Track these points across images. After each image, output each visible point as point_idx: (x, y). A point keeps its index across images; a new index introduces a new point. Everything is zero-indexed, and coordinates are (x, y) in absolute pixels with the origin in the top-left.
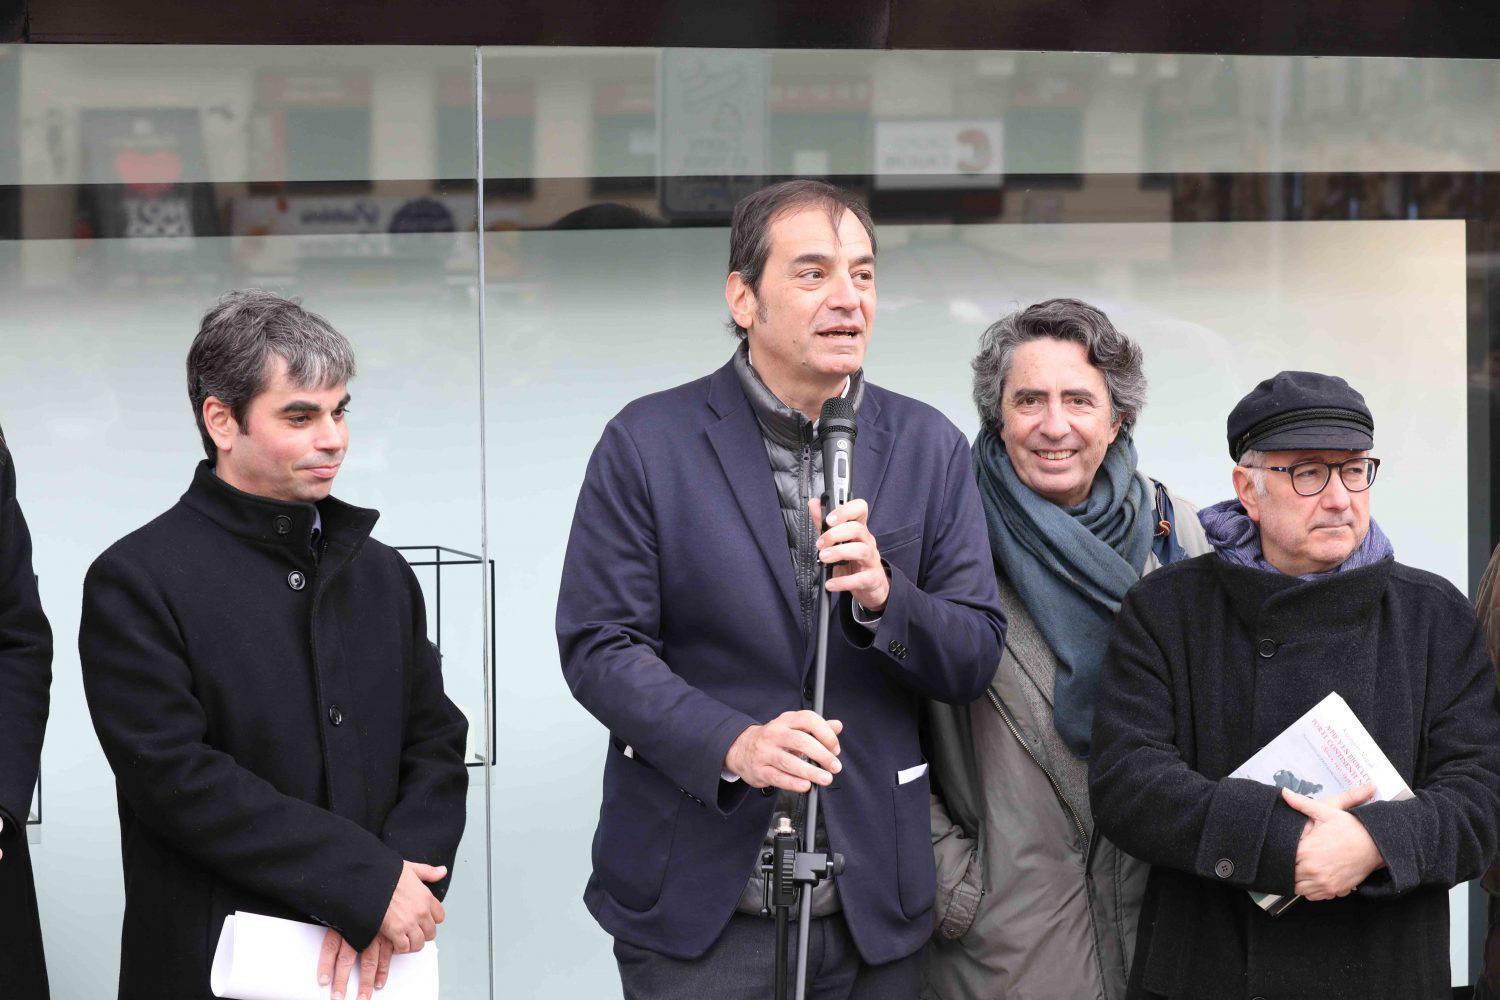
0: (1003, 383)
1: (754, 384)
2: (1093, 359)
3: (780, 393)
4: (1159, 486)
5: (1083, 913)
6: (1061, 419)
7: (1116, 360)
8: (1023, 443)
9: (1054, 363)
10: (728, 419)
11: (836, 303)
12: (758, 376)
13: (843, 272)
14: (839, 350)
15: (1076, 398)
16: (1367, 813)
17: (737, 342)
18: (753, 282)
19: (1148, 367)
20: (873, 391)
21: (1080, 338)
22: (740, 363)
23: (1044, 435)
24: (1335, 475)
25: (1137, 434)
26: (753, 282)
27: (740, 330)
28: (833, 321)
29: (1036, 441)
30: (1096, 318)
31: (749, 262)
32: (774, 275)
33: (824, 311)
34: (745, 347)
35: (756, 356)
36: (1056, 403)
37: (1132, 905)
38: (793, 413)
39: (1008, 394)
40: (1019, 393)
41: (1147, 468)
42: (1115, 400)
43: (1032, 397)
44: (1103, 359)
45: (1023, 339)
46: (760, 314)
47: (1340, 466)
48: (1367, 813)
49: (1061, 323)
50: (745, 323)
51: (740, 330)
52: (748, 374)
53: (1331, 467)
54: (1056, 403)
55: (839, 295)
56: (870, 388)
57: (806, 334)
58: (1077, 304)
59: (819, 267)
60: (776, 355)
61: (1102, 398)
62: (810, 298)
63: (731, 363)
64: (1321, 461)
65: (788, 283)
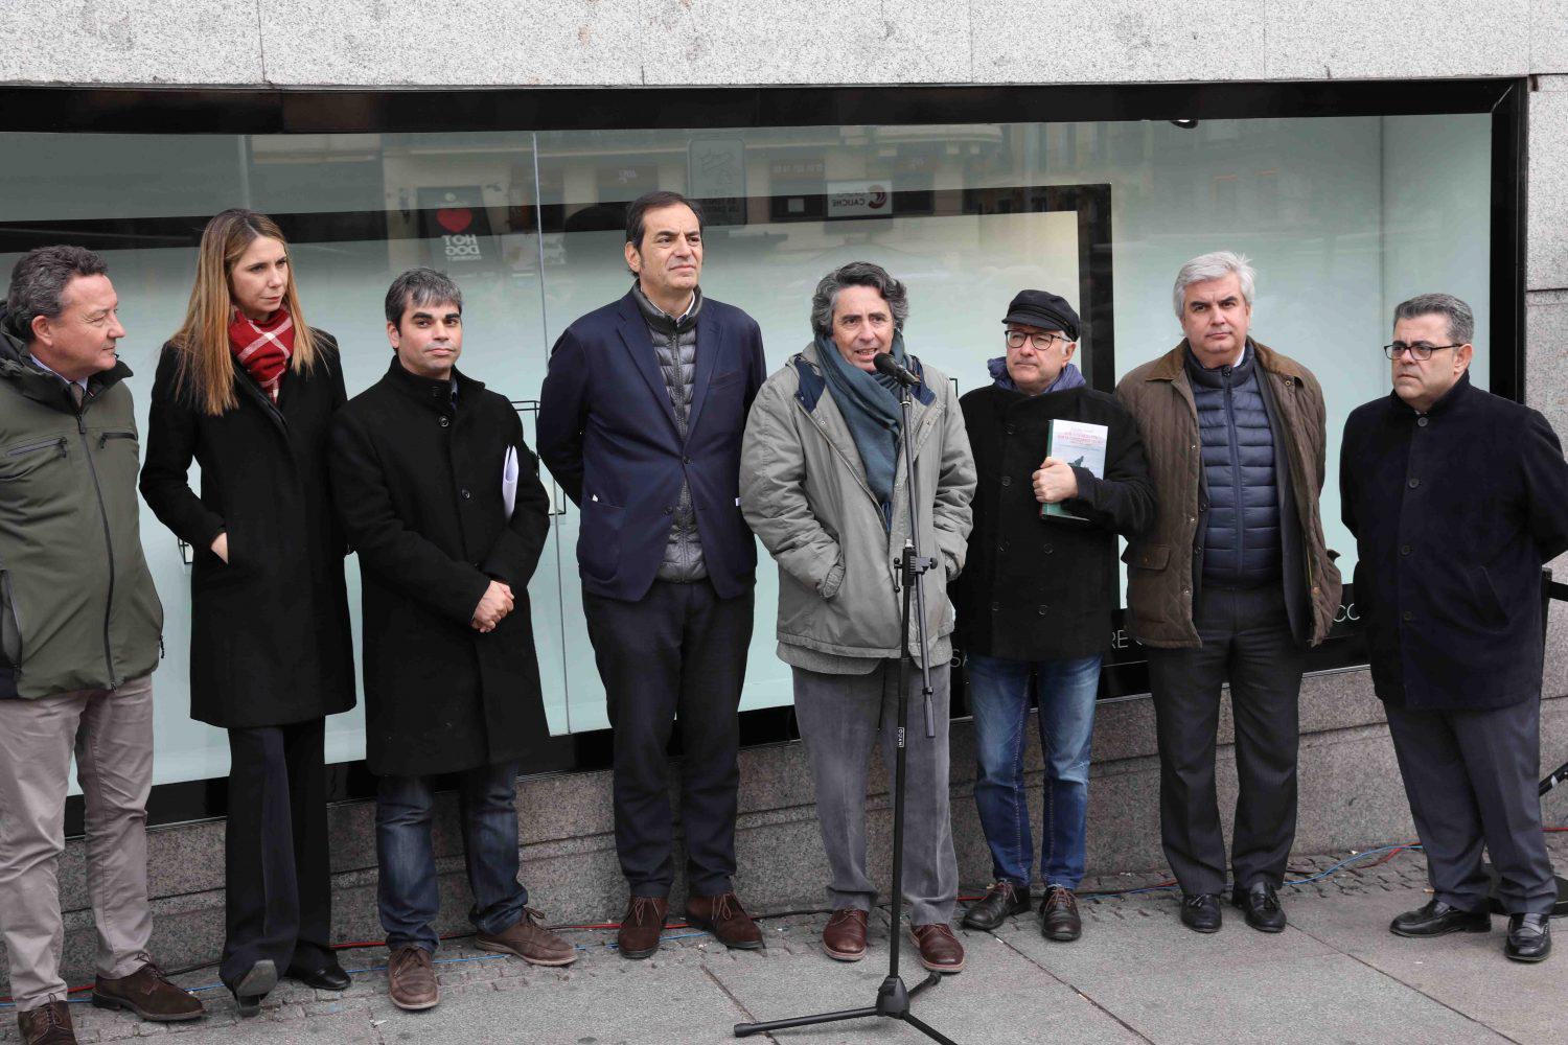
0: (833, 312)
1: (643, 301)
2: (883, 295)
3: (658, 306)
4: (914, 357)
5: (41, 688)
6: (870, 330)
7: (894, 294)
8: (849, 346)
9: (863, 299)
10: (632, 316)
11: (678, 253)
12: (646, 297)
13: (682, 238)
14: (685, 275)
15: (876, 318)
16: (1081, 473)
17: (633, 281)
18: (638, 246)
19: (909, 296)
20: (709, 303)
21: (875, 284)
22: (636, 291)
23: (862, 340)
24: (1029, 338)
25: (906, 333)
26: (638, 246)
27: (636, 274)
28: (676, 263)
29: (858, 345)
30: (879, 271)
31: (637, 236)
32: (647, 241)
33: (673, 258)
34: (638, 283)
35: (644, 288)
36: (866, 323)
37: (1424, 386)
38: (667, 316)
39: (837, 318)
40: (845, 318)
41: (909, 351)
42: (895, 317)
43: (854, 319)
44: (889, 294)
45: (843, 287)
46: (642, 264)
47: (1031, 335)
48: (1081, 473)
49: (864, 277)
50: (637, 270)
51: (636, 274)
52: (641, 296)
53: (1027, 334)
54: (866, 323)
55: (679, 249)
56: (704, 299)
57: (665, 271)
58: (868, 265)
59: (670, 237)
60: (652, 283)
61: (889, 316)
62: (664, 252)
63: (631, 292)
64: (1022, 331)
65: (653, 245)
